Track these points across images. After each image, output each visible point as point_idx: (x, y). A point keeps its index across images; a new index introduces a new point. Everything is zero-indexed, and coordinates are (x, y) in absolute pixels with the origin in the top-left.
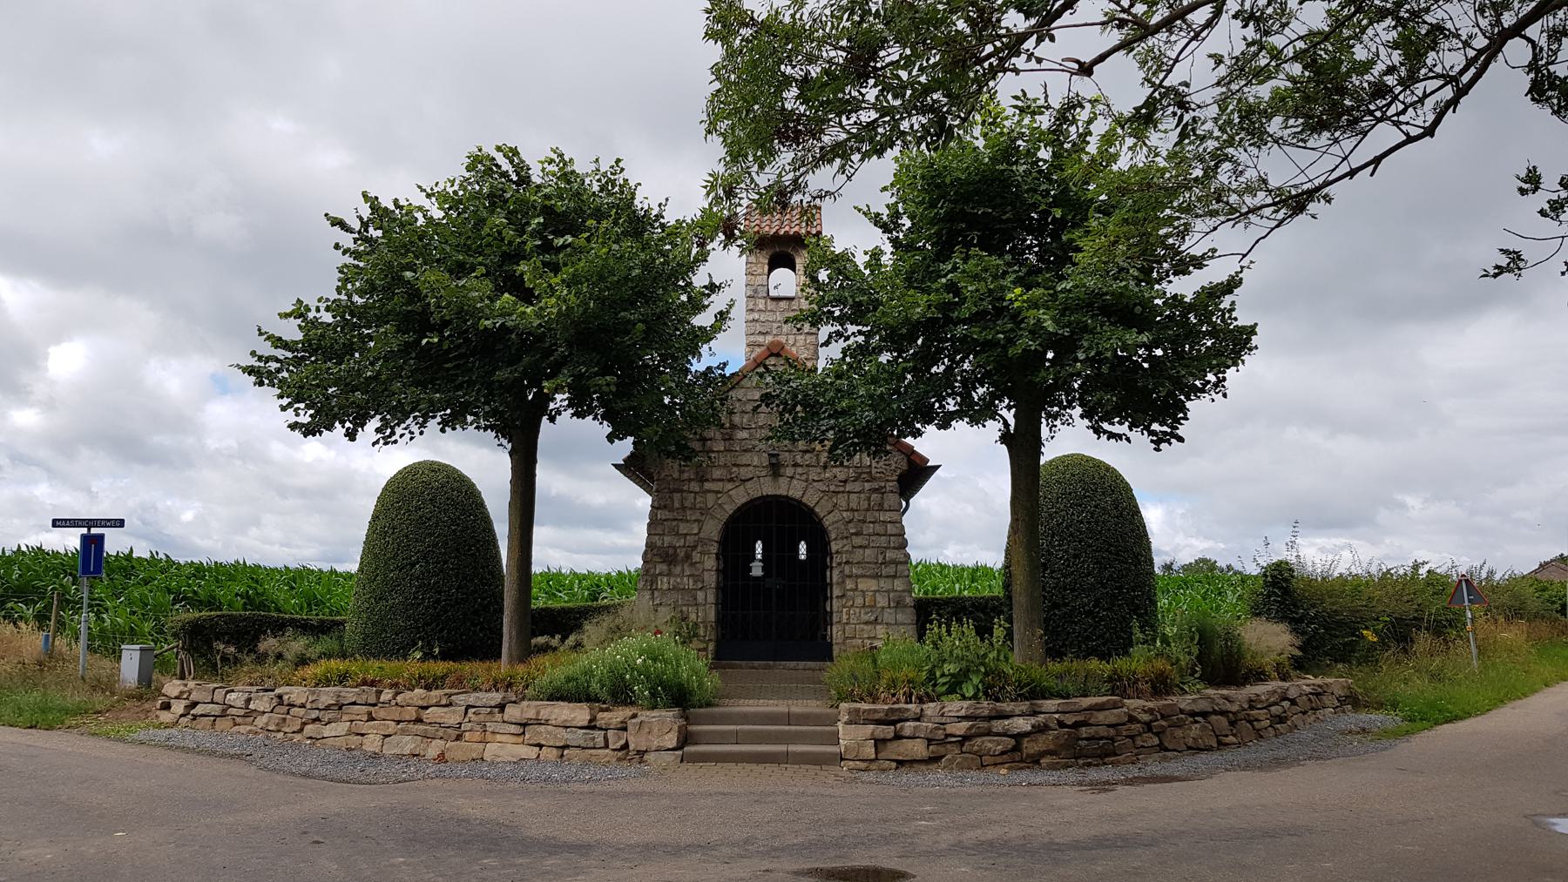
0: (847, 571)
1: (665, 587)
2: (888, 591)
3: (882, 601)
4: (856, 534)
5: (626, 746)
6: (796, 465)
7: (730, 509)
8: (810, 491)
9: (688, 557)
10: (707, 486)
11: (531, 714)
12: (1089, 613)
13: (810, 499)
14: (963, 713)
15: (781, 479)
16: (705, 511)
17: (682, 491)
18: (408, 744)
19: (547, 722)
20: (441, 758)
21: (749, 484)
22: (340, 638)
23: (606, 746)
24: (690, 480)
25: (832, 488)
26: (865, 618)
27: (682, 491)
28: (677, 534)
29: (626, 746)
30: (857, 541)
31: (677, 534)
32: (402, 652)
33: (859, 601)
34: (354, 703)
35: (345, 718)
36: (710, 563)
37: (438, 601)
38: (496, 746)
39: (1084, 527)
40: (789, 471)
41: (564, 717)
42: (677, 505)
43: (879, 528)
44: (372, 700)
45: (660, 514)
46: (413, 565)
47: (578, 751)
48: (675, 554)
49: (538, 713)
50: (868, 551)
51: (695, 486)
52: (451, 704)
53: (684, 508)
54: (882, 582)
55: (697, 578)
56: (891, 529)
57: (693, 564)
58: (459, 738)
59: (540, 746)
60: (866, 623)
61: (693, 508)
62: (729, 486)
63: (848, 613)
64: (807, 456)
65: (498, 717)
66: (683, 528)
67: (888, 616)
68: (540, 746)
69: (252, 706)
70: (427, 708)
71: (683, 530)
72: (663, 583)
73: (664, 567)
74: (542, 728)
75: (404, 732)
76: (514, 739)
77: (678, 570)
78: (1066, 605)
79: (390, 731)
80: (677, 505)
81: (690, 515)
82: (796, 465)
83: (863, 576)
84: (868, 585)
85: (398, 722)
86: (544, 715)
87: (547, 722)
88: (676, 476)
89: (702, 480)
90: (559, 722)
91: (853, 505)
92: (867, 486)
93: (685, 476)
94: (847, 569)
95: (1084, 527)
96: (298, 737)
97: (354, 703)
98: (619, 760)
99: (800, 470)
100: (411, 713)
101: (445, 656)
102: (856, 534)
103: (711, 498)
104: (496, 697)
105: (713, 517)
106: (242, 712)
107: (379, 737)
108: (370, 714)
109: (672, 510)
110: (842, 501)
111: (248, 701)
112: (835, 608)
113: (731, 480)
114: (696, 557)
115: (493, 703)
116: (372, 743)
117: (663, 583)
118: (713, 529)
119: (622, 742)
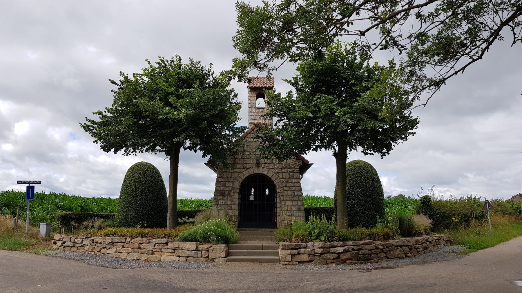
0: (282, 198)
1: (221, 204)
3: (294, 209)
5: (208, 257)
6: (265, 163)
7: (243, 178)
8: (270, 172)
9: (229, 194)
10: (235, 170)
11: (177, 246)
12: (362, 213)
14: (320, 246)
15: (260, 168)
16: (235, 178)
18: (135, 256)
19: (182, 249)
20: (147, 260)
23: (202, 257)
25: (277, 171)
26: (288, 214)
29: (208, 257)
30: (285, 188)
31: (225, 186)
33: (286, 208)
34: (118, 242)
35: (115, 247)
36: (237, 196)
37: (146, 208)
38: (165, 256)
40: (263, 165)
42: (225, 176)
44: (124, 241)
46: (137, 196)
47: (192, 258)
49: (179, 245)
50: (289, 192)
53: (227, 177)
54: (294, 202)
55: (232, 201)
57: (230, 196)
58: (152, 254)
59: (180, 256)
60: (288, 216)
62: (243, 170)
63: (282, 213)
65: (166, 247)
67: (296, 213)
68: (180, 256)
69: (83, 243)
70: (142, 244)
72: (221, 202)
74: (180, 251)
76: (171, 254)
77: (226, 198)
78: (355, 210)
79: (130, 251)
80: (225, 176)
82: (265, 163)
84: (289, 203)
85: (132, 248)
86: (181, 246)
87: (182, 249)
92: (289, 170)
94: (282, 198)
96: (99, 253)
97: (118, 242)
98: (206, 261)
99: (266, 165)
100: (136, 245)
101: (148, 226)
102: (285, 186)
103: (237, 174)
104: (165, 240)
105: (237, 181)
106: (80, 245)
107: (126, 254)
108: (123, 246)
109: (224, 178)
110: (280, 175)
111: (82, 241)
113: (243, 168)
114: (232, 194)
116: (123, 255)
117: (221, 202)
118: (237, 185)
119: (207, 255)
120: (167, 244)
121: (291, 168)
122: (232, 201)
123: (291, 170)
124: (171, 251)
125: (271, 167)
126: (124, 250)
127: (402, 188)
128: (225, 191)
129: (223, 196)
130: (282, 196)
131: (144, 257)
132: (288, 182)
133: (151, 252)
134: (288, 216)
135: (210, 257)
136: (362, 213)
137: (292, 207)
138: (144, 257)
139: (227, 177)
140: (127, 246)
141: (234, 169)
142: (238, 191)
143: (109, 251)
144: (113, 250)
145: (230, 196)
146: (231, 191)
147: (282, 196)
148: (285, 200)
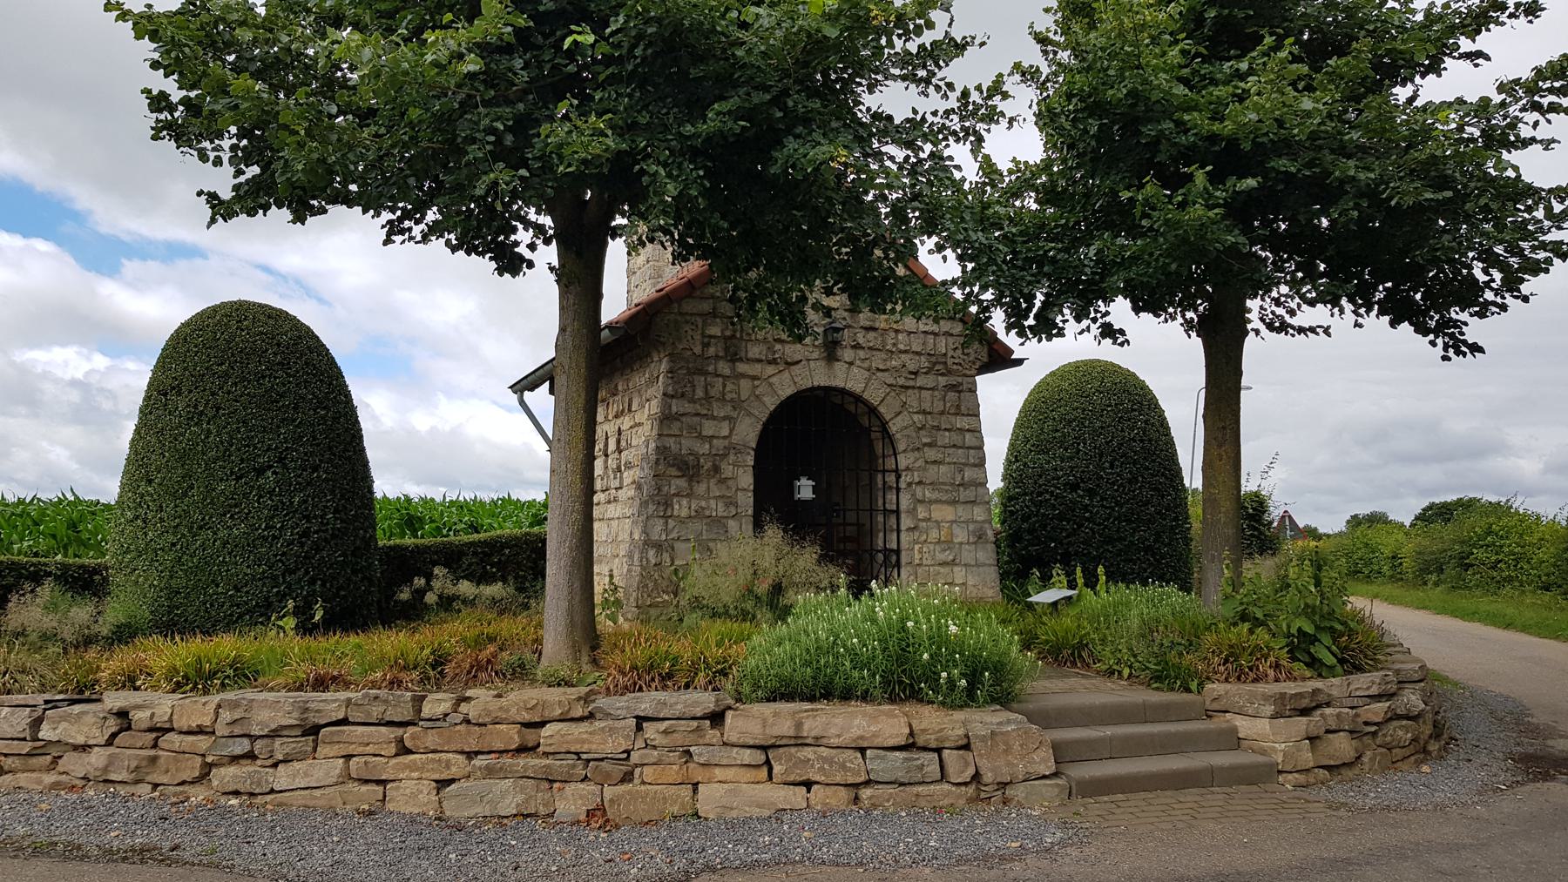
0: (919, 495)
1: (684, 513)
2: (966, 522)
3: (961, 535)
4: (930, 445)
5: (977, 777)
6: (857, 347)
7: (771, 403)
8: (874, 384)
9: (716, 469)
10: (742, 367)
11: (785, 728)
12: (1147, 549)
13: (874, 395)
14: (1374, 690)
15: (838, 365)
16: (737, 404)
17: (706, 373)
18: (508, 797)
19: (817, 742)
20: (597, 813)
21: (796, 369)
22: (1236, 584)
23: (943, 776)
24: (717, 357)
25: (901, 381)
26: (941, 557)
27: (706, 373)
28: (700, 437)
29: (977, 777)
30: (931, 454)
31: (700, 437)
32: (260, 613)
33: (934, 534)
34: (344, 722)
35: (323, 750)
36: (746, 479)
37: (306, 534)
38: (320, 759)
39: (1137, 446)
40: (848, 354)
41: (855, 732)
42: (700, 393)
43: (956, 438)
44: (406, 714)
45: (676, 406)
46: (260, 472)
47: (891, 790)
48: (698, 466)
49: (799, 725)
50: (943, 468)
51: (724, 368)
52: (591, 716)
53: (708, 397)
54: (960, 508)
55: (730, 502)
56: (969, 439)
57: (722, 481)
58: (627, 777)
59: (808, 785)
60: (944, 564)
61: (722, 399)
62: (771, 370)
63: (920, 552)
64: (871, 335)
65: (712, 735)
66: (709, 428)
67: (968, 555)
68: (808, 785)
69: (46, 733)
70: (542, 724)
71: (707, 432)
72: (681, 508)
73: (682, 483)
74: (808, 753)
75: (490, 772)
76: (750, 774)
77: (701, 489)
78: (1121, 539)
79: (454, 771)
80: (700, 393)
81: (719, 411)
82: (857, 347)
83: (937, 501)
84: (943, 513)
85: (470, 755)
86: (811, 727)
87: (817, 742)
88: (698, 350)
89: (734, 358)
90: (845, 739)
91: (927, 406)
92: (943, 381)
93: (712, 351)
94: (919, 491)
95: (1137, 446)
96: (198, 795)
97: (344, 722)
98: (970, 801)
99: (861, 354)
100: (511, 735)
101: (333, 623)
102: (930, 445)
103: (745, 384)
104: (704, 700)
105: (749, 414)
106: (26, 747)
107: (427, 787)
108: (400, 741)
109: (693, 401)
110: (911, 398)
111: (37, 723)
112: (904, 545)
113: (773, 362)
114: (727, 470)
115: (699, 712)
116: (412, 793)
117: (681, 508)
118: (748, 431)
119: (971, 771)
120: (717, 718)
121: (949, 372)
122: (730, 502)
123: (953, 380)
124: (748, 756)
125: (877, 362)
126: (412, 767)
127: (418, 484)
128: (697, 456)
129: (691, 479)
130: (920, 483)
131: (572, 801)
132: (938, 428)
133: (618, 770)
134: (944, 564)
135: (988, 777)
136: (1147, 549)
137: (957, 530)
138: (572, 801)
139: (708, 397)
140: (432, 739)
141: (733, 361)
142: (750, 460)
143: (282, 778)
144: (323, 769)
145: (722, 481)
146: (725, 456)
147: (920, 483)
148: (931, 502)
